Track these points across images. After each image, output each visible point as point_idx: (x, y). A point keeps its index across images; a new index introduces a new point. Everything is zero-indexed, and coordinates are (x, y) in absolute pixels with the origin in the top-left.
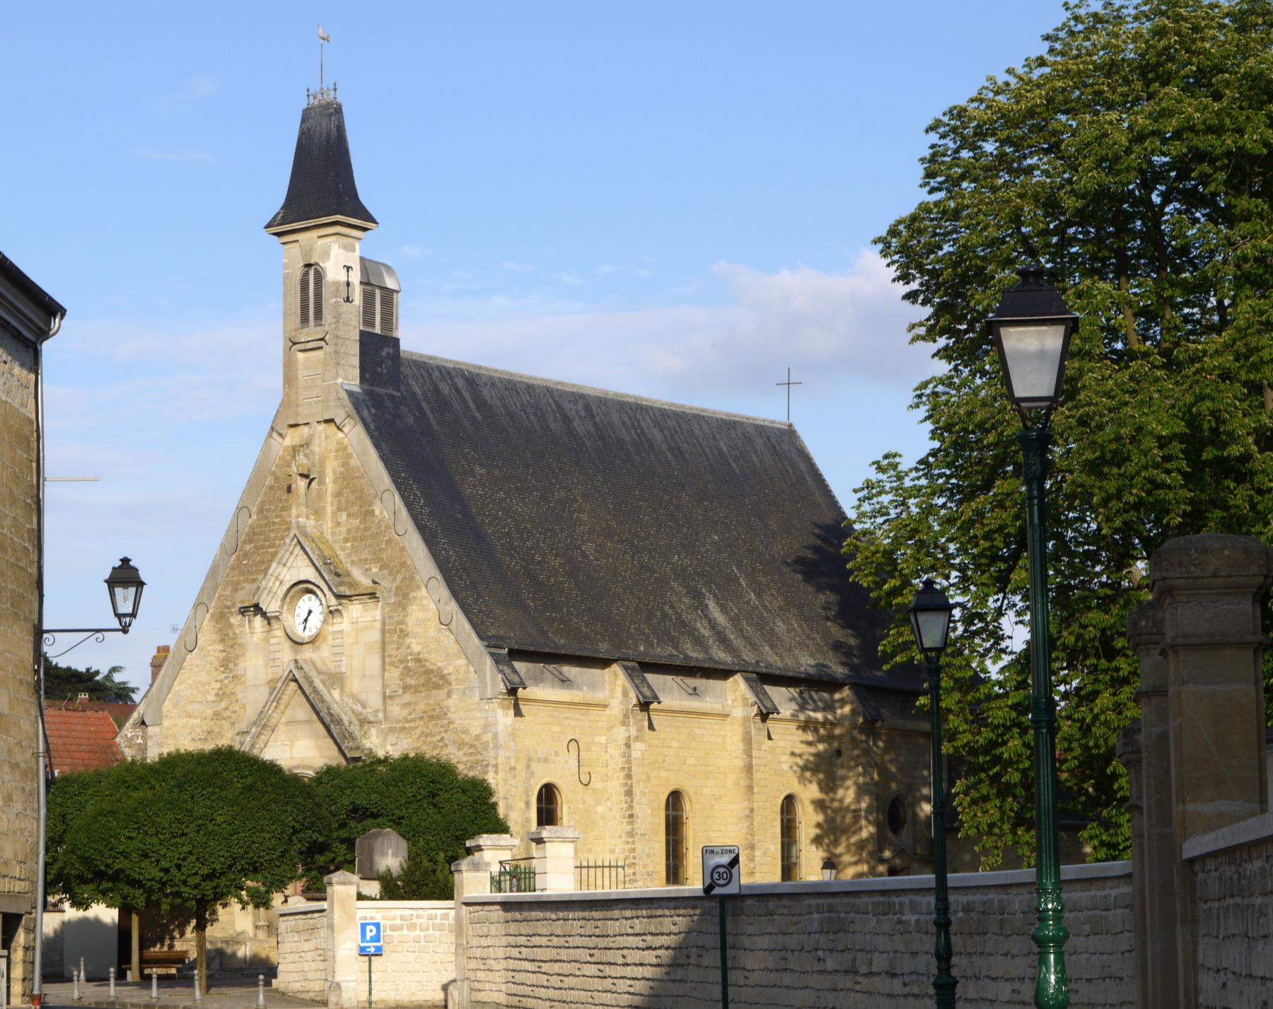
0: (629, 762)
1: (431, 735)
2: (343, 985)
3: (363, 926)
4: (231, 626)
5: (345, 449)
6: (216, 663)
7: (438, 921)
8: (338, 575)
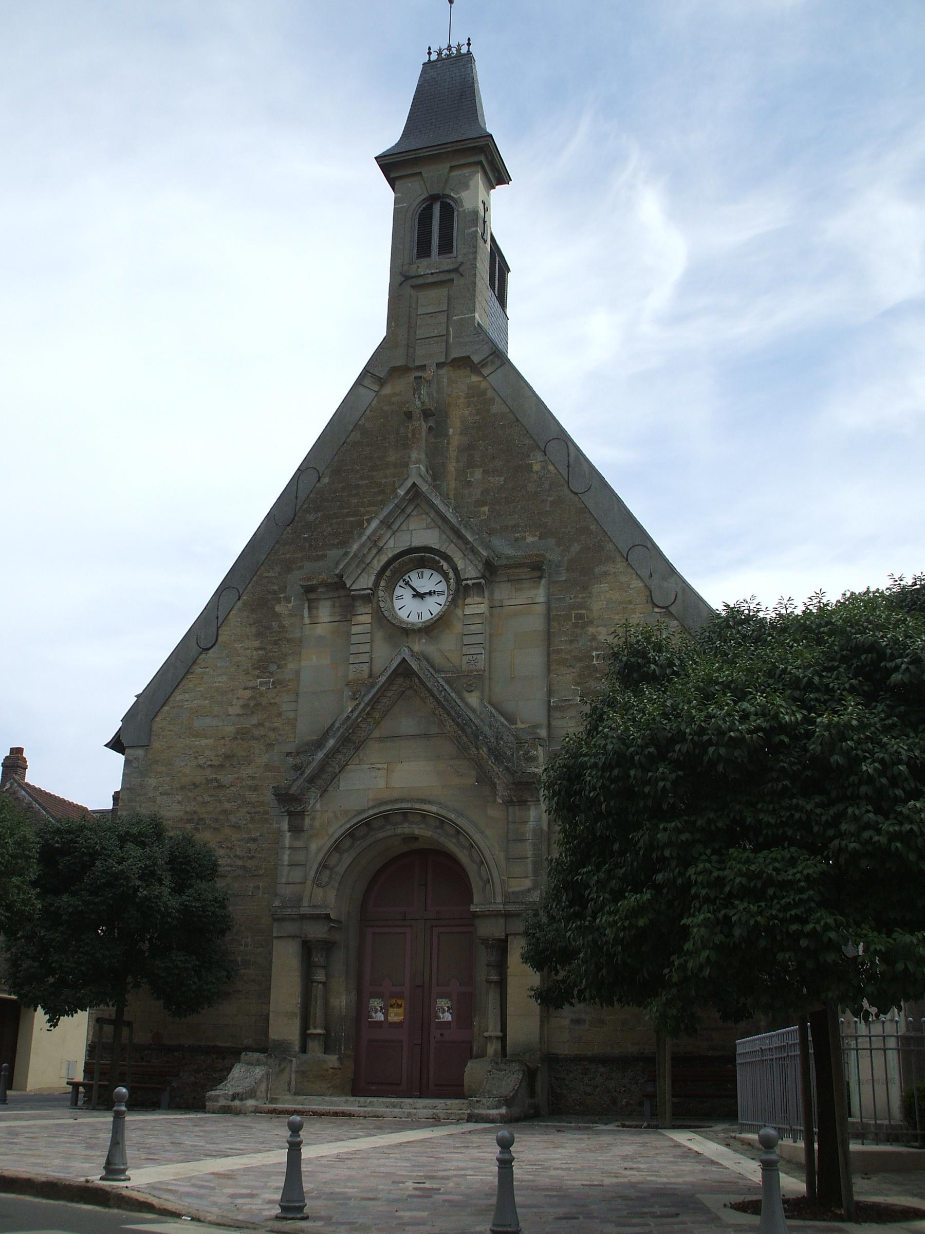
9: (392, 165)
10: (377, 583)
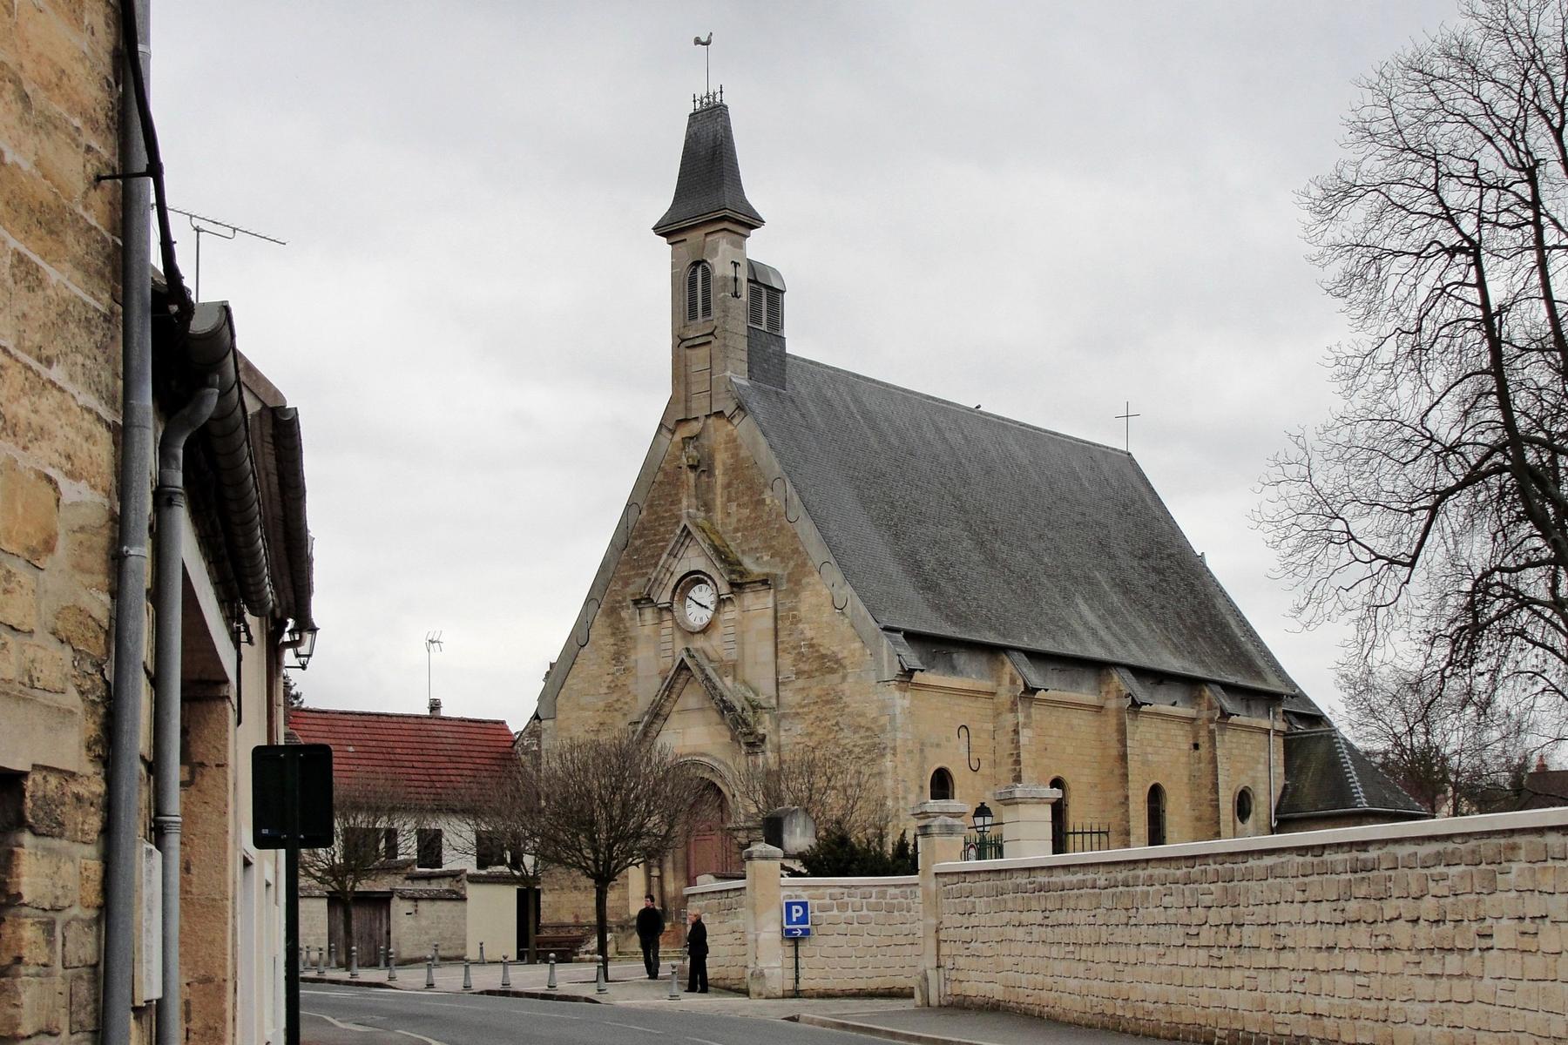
0: (1017, 747)
1: (825, 719)
2: (766, 971)
3: (789, 905)
4: (621, 620)
5: (735, 440)
6: (608, 656)
7: (873, 900)
8: (730, 564)
9: (668, 229)
10: (672, 598)
